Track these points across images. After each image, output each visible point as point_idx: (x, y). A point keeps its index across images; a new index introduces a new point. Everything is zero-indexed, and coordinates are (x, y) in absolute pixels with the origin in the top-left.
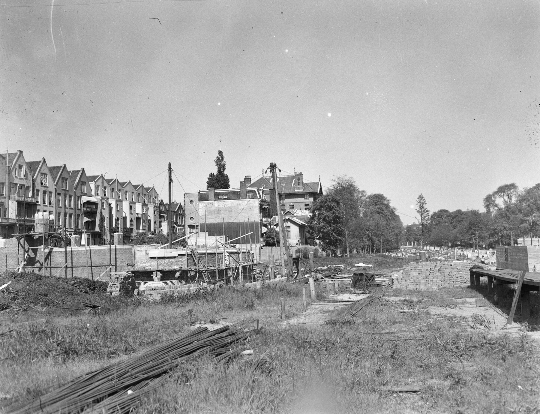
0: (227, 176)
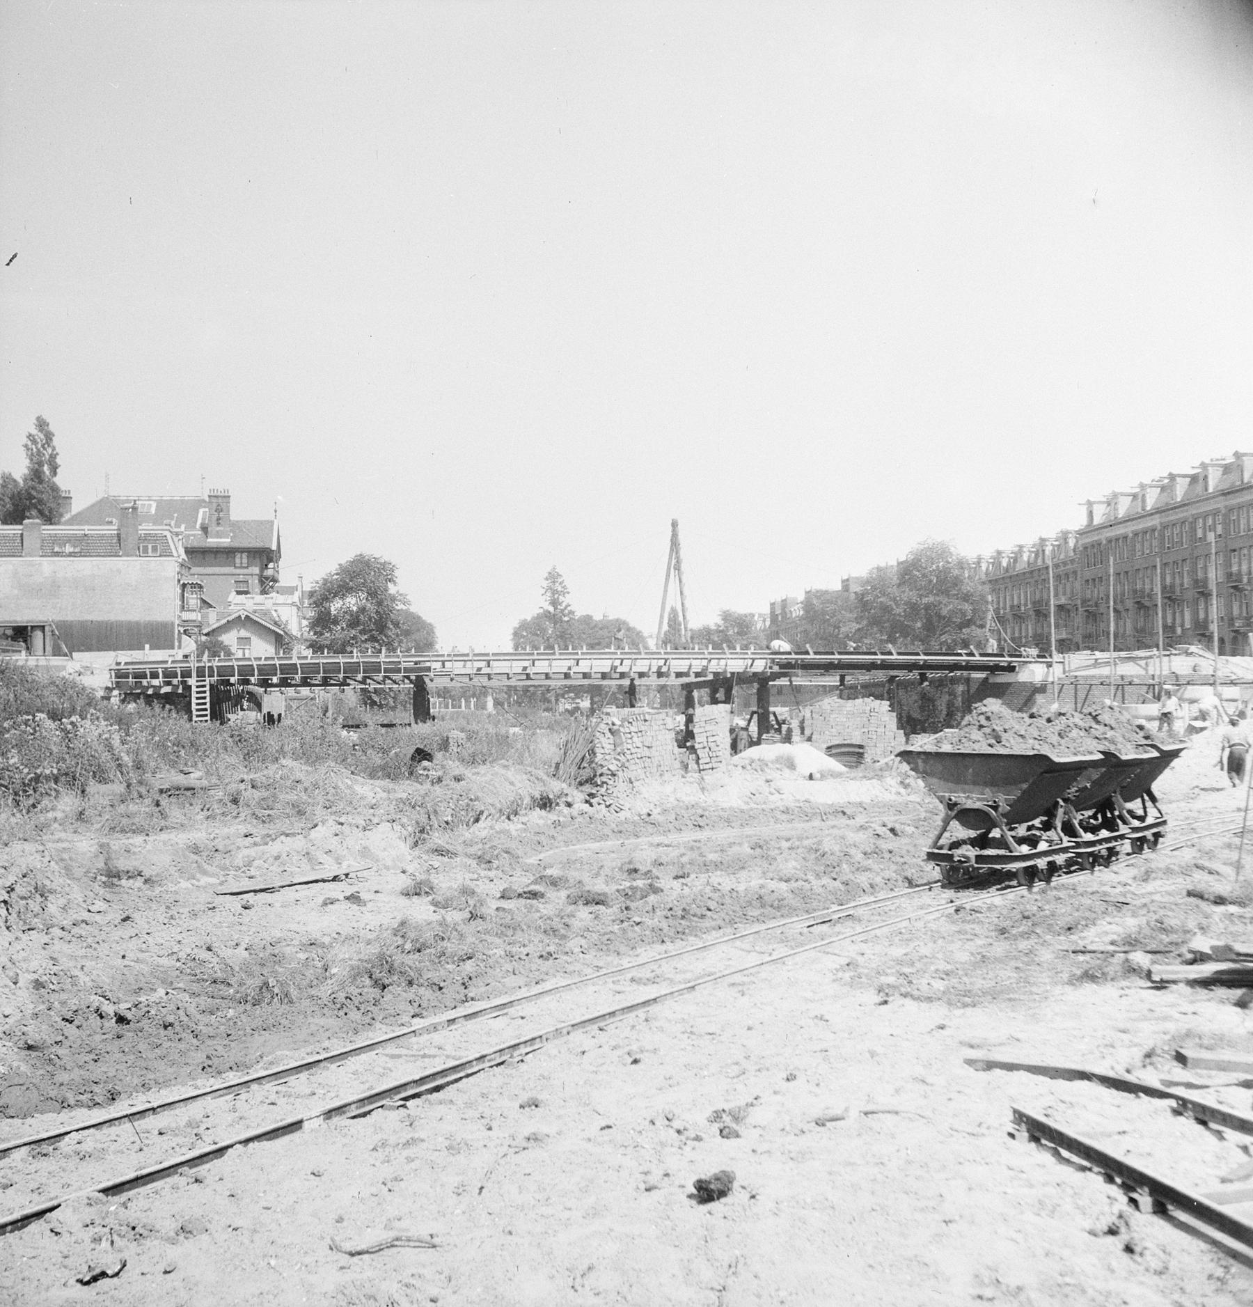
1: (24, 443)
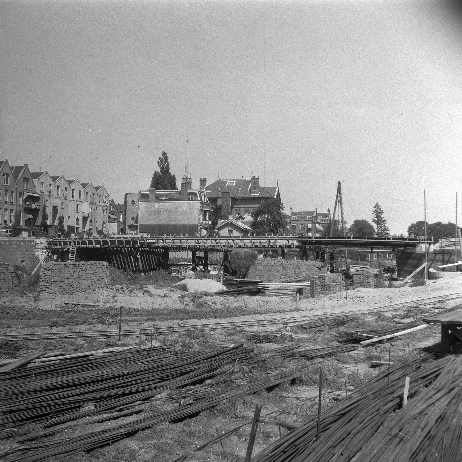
0: (174, 176)
1: (158, 161)
